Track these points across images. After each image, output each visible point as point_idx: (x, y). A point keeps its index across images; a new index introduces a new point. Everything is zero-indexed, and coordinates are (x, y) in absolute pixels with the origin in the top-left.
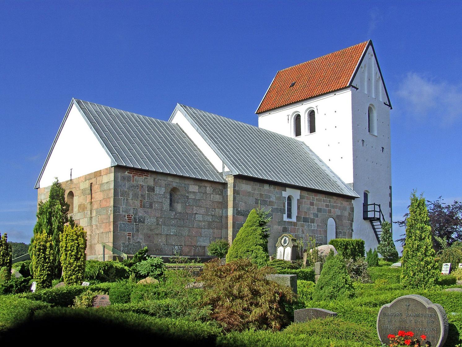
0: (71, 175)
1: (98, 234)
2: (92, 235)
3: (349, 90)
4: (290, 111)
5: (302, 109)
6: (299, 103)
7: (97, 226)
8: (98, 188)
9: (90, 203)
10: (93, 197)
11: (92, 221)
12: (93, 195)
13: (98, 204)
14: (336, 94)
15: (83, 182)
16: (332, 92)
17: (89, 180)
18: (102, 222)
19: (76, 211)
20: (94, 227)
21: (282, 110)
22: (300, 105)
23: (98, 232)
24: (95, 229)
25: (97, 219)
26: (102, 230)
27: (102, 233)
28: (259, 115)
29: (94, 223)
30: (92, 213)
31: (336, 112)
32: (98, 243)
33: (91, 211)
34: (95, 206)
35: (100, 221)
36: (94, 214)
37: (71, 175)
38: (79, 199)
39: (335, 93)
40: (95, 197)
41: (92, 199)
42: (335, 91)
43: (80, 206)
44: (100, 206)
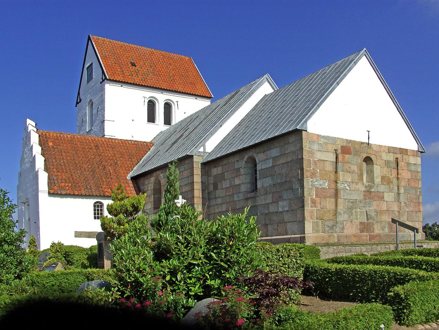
0: (369, 138)
1: (408, 212)
2: (401, 211)
3: (210, 101)
4: (148, 94)
5: (161, 98)
6: (159, 91)
7: (405, 203)
8: (404, 166)
9: (396, 178)
10: (399, 173)
11: (400, 197)
12: (400, 171)
13: (406, 182)
14: (123, 86)
15: (386, 153)
16: (195, 95)
17: (393, 154)
18: (412, 201)
19: (378, 182)
20: (403, 204)
21: (112, 84)
22: (159, 93)
23: (407, 210)
24: (403, 206)
25: (406, 197)
26: (411, 209)
27: (412, 211)
28: (109, 82)
29: (402, 199)
30: (399, 189)
31: (185, 113)
32: (408, 221)
33: (398, 187)
34: (403, 184)
35: (409, 199)
36: (402, 191)
37: (369, 138)
38: (381, 170)
39: (162, 92)
40: (402, 174)
41: (399, 175)
42: (198, 96)
43: (383, 178)
44: (408, 184)
